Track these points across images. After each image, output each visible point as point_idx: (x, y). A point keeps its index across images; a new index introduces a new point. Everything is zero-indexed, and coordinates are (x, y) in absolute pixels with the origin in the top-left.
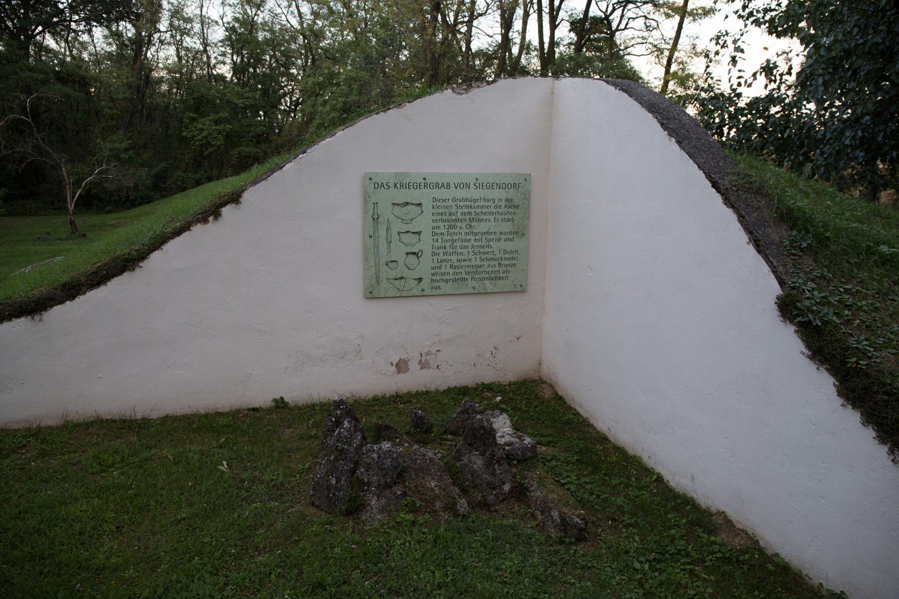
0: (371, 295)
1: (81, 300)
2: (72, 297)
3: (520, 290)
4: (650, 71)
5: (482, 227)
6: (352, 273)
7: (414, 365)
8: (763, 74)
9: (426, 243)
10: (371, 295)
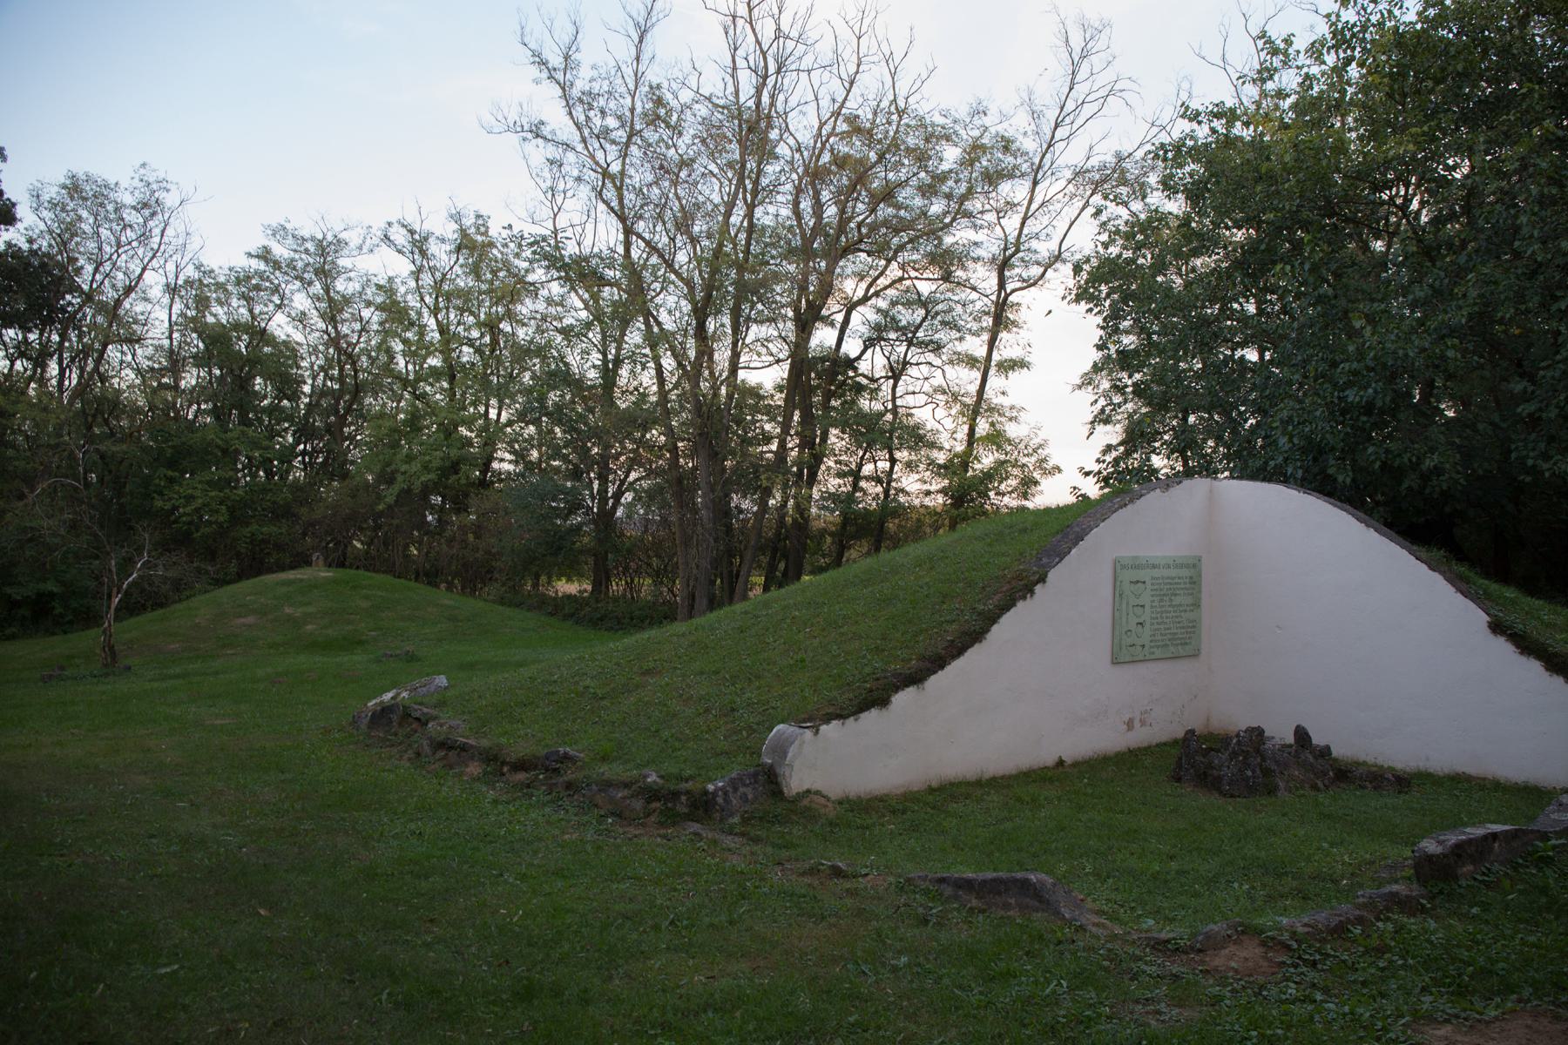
0: (1115, 662)
1: (948, 669)
2: (942, 667)
3: (1195, 655)
4: (966, 428)
5: (1177, 600)
6: (1102, 645)
7: (1137, 724)
8: (25, 247)
9: (1146, 616)
10: (1115, 662)
